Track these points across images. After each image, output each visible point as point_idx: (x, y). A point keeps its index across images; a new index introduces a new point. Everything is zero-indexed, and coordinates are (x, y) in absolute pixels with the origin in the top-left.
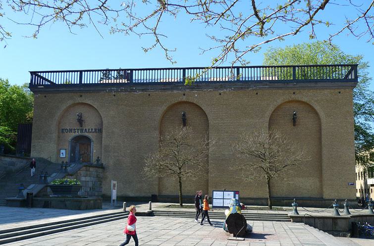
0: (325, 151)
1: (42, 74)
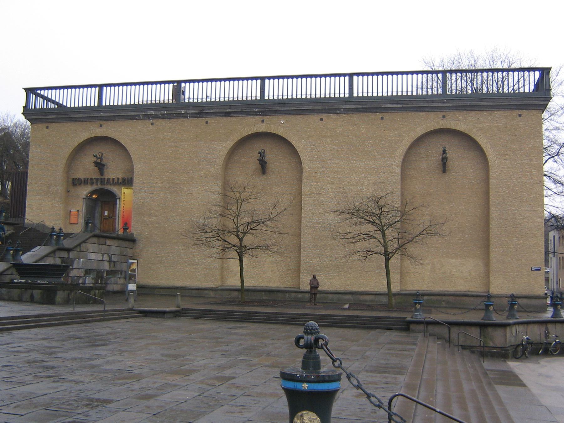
0: (494, 213)
1: (42, 92)
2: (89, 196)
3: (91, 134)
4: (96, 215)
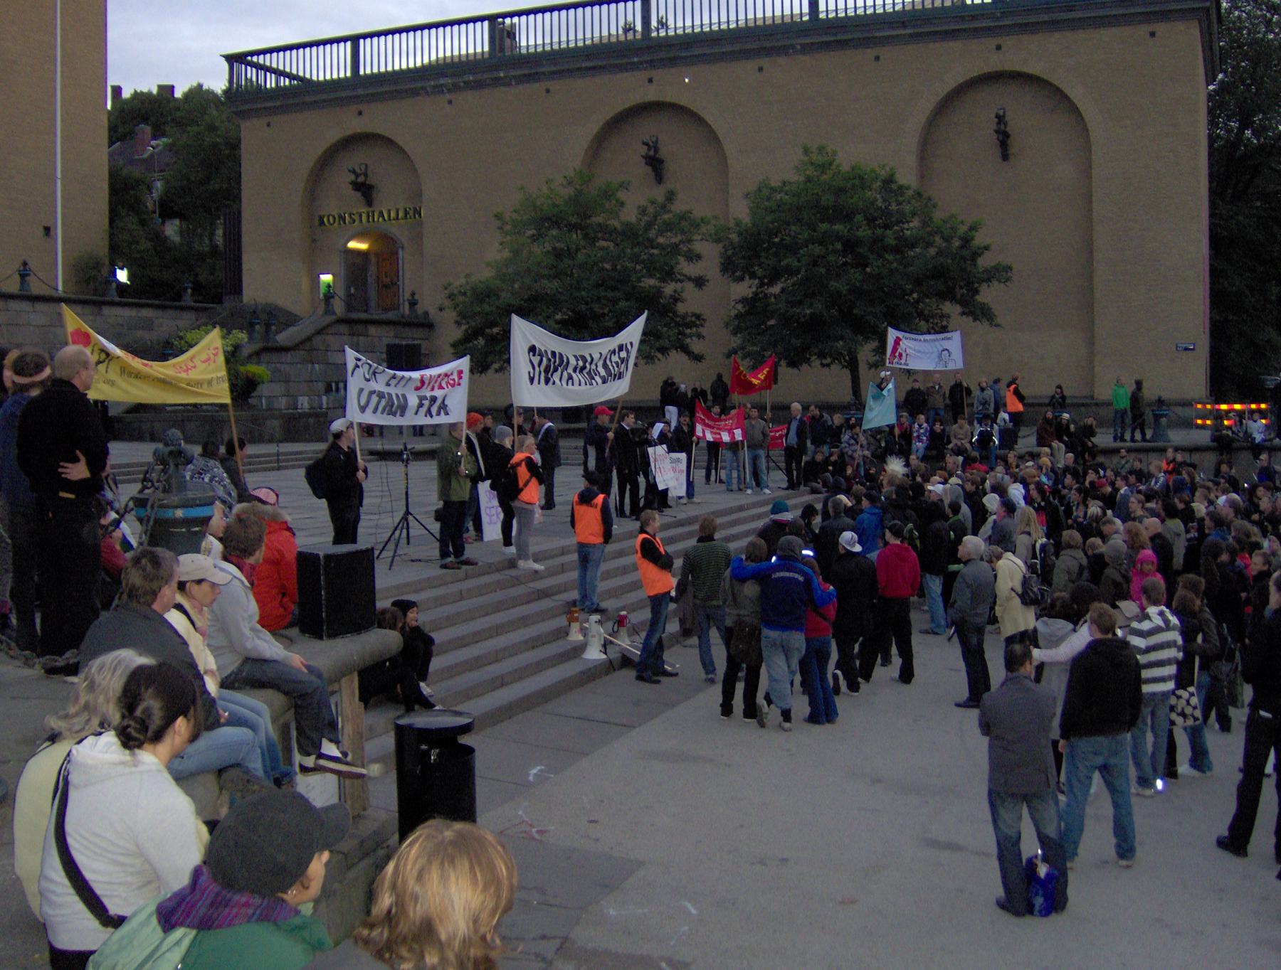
1: (261, 59)
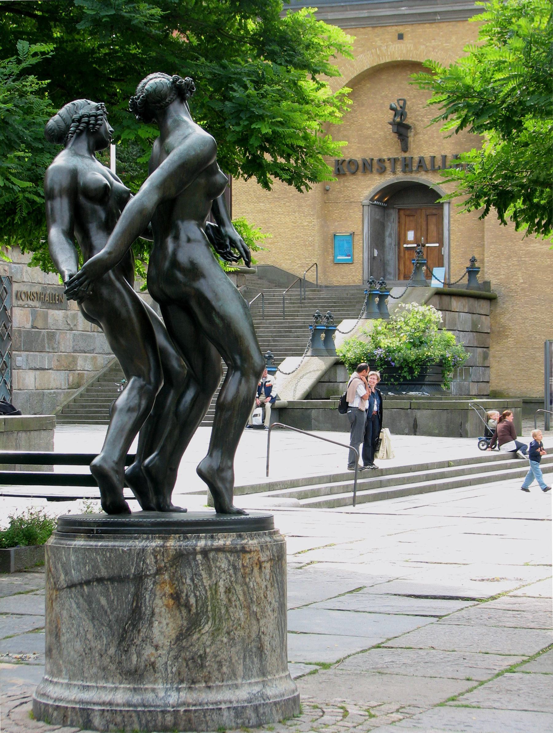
2: (377, 200)
3: (378, 56)
4: (388, 241)
